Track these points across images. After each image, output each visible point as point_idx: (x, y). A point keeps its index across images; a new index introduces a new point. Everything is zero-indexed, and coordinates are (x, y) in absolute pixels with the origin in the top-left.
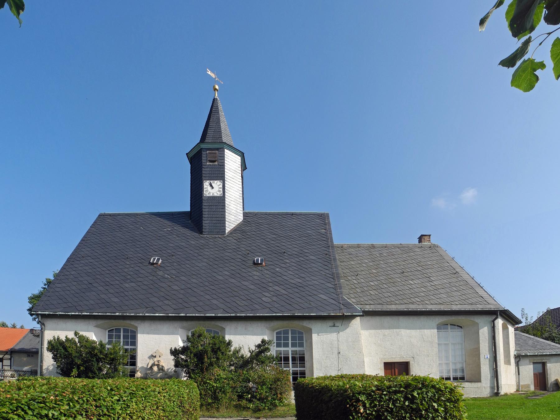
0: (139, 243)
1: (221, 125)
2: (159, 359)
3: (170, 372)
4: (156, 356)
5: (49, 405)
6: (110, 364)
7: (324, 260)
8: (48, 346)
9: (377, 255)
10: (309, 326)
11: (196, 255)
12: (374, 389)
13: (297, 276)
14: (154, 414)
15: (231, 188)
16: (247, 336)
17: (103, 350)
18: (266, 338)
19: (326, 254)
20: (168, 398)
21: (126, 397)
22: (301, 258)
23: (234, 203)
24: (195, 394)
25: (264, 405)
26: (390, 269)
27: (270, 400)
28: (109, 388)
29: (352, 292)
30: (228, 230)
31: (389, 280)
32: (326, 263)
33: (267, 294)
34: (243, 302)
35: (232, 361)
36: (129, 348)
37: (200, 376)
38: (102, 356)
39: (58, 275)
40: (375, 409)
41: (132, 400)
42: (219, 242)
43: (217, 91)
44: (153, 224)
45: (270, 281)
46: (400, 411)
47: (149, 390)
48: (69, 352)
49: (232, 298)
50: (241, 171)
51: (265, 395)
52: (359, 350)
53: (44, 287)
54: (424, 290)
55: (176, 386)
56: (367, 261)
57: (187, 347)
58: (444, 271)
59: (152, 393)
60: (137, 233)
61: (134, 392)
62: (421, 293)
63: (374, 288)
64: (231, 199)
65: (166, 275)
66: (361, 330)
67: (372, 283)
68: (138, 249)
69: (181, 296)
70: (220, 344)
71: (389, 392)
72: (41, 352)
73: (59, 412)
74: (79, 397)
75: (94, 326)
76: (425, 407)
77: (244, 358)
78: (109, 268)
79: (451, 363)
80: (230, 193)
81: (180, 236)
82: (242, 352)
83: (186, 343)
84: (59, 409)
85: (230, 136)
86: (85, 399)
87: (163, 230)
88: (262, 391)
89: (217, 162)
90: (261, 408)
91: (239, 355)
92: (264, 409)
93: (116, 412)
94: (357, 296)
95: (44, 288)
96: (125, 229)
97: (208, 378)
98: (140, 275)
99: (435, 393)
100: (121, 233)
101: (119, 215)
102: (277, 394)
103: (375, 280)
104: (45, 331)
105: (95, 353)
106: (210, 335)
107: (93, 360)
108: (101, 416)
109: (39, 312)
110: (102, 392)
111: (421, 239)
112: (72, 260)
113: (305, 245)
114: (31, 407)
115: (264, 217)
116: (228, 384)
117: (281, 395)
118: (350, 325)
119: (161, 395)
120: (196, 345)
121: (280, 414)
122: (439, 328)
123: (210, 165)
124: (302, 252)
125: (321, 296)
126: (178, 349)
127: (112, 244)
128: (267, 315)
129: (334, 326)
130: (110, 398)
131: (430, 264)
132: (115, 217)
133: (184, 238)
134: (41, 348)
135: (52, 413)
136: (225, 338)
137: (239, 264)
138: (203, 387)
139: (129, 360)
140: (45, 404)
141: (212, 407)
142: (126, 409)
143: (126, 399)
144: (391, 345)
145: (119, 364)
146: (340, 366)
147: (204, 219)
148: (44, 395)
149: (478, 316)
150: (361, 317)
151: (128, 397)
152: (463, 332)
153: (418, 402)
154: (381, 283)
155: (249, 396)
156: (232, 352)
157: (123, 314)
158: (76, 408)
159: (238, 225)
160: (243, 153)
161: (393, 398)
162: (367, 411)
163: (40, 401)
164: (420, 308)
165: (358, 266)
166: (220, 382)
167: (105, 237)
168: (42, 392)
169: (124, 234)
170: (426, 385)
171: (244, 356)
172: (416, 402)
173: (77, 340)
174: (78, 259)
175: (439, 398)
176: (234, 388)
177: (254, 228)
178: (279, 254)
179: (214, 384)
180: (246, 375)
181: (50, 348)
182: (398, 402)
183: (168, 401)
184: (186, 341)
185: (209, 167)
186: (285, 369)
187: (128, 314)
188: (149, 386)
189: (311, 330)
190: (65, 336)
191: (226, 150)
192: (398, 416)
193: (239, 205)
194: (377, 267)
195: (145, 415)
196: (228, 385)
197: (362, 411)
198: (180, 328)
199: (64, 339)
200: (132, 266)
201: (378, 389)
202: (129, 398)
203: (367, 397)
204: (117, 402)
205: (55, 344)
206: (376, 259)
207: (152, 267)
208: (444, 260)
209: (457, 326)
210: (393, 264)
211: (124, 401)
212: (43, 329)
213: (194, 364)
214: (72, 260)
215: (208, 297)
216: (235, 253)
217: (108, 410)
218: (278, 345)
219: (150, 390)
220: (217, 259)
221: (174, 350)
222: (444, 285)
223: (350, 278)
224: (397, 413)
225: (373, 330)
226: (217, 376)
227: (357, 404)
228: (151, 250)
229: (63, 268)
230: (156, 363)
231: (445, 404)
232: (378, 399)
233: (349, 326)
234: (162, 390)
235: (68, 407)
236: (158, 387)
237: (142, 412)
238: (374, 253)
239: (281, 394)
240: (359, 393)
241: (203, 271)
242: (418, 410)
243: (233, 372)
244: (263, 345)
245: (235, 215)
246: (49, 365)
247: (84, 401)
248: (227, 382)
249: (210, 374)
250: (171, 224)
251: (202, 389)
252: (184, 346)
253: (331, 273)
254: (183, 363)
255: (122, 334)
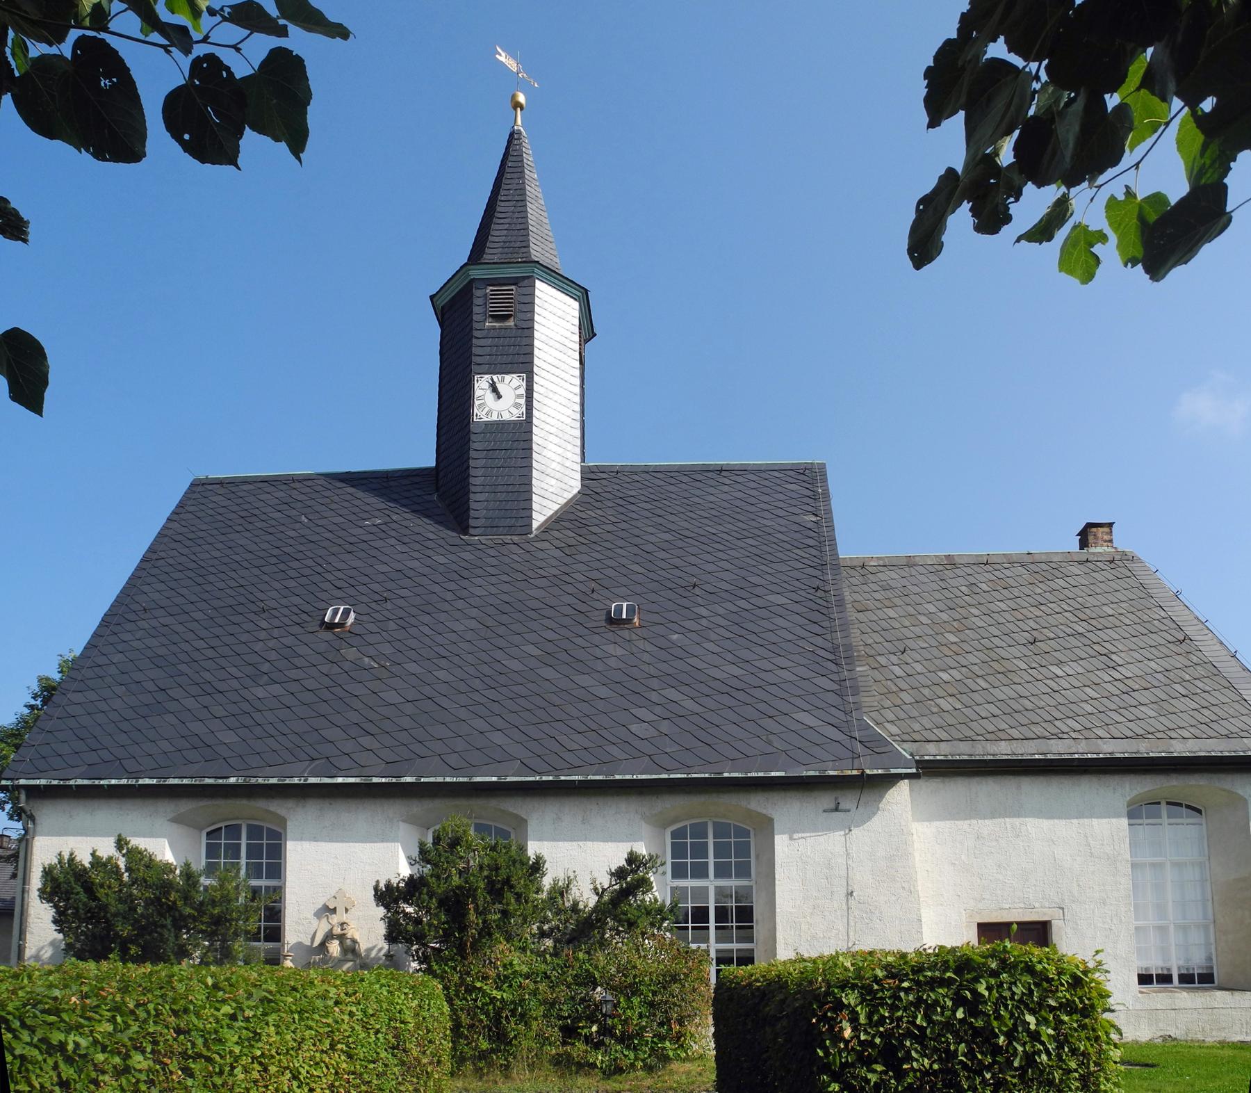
0: (295, 564)
1: (529, 209)
2: (344, 919)
3: (374, 958)
4: (335, 908)
5: (67, 1020)
6: (210, 936)
7: (810, 604)
8: (44, 885)
9: (963, 589)
10: (764, 812)
11: (449, 596)
12: (880, 973)
13: (730, 657)
14: (324, 1062)
15: (551, 395)
16: (589, 844)
17: (193, 893)
18: (642, 849)
19: (817, 589)
20: (362, 1019)
21: (251, 1010)
22: (742, 603)
23: (556, 440)
24: (436, 1015)
25: (632, 1055)
26: (997, 633)
27: (650, 1039)
28: (210, 981)
29: (887, 703)
30: (538, 519)
31: (992, 664)
32: (816, 617)
33: (641, 713)
34: (577, 737)
35: (545, 920)
36: (261, 887)
37: (455, 969)
38: (188, 911)
39: (75, 667)
40: (881, 1029)
41: (266, 1018)
42: (513, 556)
43: (522, 109)
44: (333, 506)
45: (653, 671)
46: (944, 1036)
47: (311, 993)
48: (99, 900)
49: (545, 727)
50: (580, 345)
51: (636, 1025)
52: (906, 885)
53: (33, 702)
54: (1093, 694)
55: (384, 988)
56: (932, 608)
57: (421, 878)
58: (1151, 635)
59: (319, 1003)
60: (292, 533)
61: (271, 997)
62: (1083, 705)
63: (952, 690)
64: (548, 428)
65: (366, 660)
66: (914, 820)
67: (945, 676)
68: (292, 583)
69: (406, 722)
70: (512, 868)
71: (918, 983)
72: (22, 906)
73: (91, 1038)
74: (137, 1001)
75: (169, 820)
76: (1006, 1025)
77: (580, 910)
78: (215, 642)
79: (1172, 926)
80: (545, 409)
81: (406, 540)
82: (574, 893)
83: (417, 866)
84: (92, 1032)
85: (550, 239)
86: (151, 1006)
87: (360, 523)
88: (629, 1013)
89: (512, 319)
90: (625, 1063)
91: (567, 904)
92: (632, 1065)
93: (227, 1049)
94: (902, 715)
95: (32, 707)
96: (259, 525)
97: (478, 973)
98: (296, 661)
99: (1032, 987)
100: (248, 535)
101: (245, 481)
102: (669, 1020)
103: (954, 664)
104: (36, 838)
105: (170, 901)
106: (482, 840)
107: (165, 922)
108: (188, 1059)
109: (22, 782)
110: (194, 991)
111: (1085, 536)
112: (116, 620)
113: (754, 563)
114: (28, 1022)
115: (639, 479)
116: (535, 993)
117: (680, 1025)
118: (880, 805)
119: (342, 1012)
120: (446, 870)
121: (678, 1082)
122: (1134, 812)
123: (494, 328)
124: (743, 584)
125: (801, 716)
126: (395, 885)
127: (224, 568)
128: (644, 777)
129: (836, 810)
130: (212, 1010)
131: (1111, 612)
132: (233, 489)
133: (417, 546)
134: (23, 891)
135: (74, 1041)
136: (526, 850)
137: (567, 621)
138: (464, 1002)
139: (262, 924)
140: (59, 1017)
141: (491, 1065)
142: (252, 1042)
143: (251, 1014)
144: (999, 866)
145: (236, 934)
146: (851, 934)
147: (472, 489)
148: (57, 993)
149: (963, 778)
150: (914, 781)
151: (257, 1008)
152: (1204, 825)
153: (989, 1011)
154: (970, 674)
155: (594, 1028)
156: (545, 894)
157: (248, 779)
158: (131, 1031)
159: (566, 504)
160: (586, 291)
161: (926, 1000)
162: (862, 1034)
163: (47, 1006)
164: (1081, 749)
165: (907, 624)
166: (510, 986)
167: (207, 547)
168: (51, 986)
169: (257, 539)
170: (1011, 962)
171: (581, 906)
172: (982, 1012)
173: (122, 863)
174: (132, 617)
175: (1042, 999)
176: (552, 1005)
177: (610, 511)
178: (681, 591)
179: (494, 992)
180: (584, 963)
181: (48, 890)
182: (939, 1010)
183: (360, 1029)
184: (417, 859)
185: (490, 335)
186: (694, 946)
187: (260, 781)
188: (312, 983)
189: (770, 821)
190: (91, 852)
191: (538, 284)
192: (939, 1050)
193: (569, 447)
194: (962, 627)
195: (301, 1066)
196: (535, 995)
197: (847, 1033)
198: (403, 821)
199: (85, 859)
200: (276, 633)
201: (893, 976)
202: (259, 1013)
203: (862, 994)
204: (228, 1022)
205: (62, 876)
206: (958, 601)
207: (327, 635)
208: (1152, 601)
209: (1188, 807)
210: (1007, 615)
211: (247, 1020)
212: (31, 832)
213: (439, 932)
214: (116, 620)
215: (479, 724)
216: (555, 591)
217: (206, 1044)
218: (678, 872)
219: (314, 992)
220: (507, 608)
221: (384, 889)
222: (1149, 678)
223: (882, 660)
224: (935, 1040)
225: (947, 822)
226: (505, 966)
227: (838, 1015)
228: (327, 586)
229: (90, 646)
230: (337, 931)
231: (1057, 1018)
232: (889, 1002)
233: (878, 809)
234: (346, 994)
235: (110, 1028)
236: (335, 987)
237: (292, 1056)
238: (953, 582)
239: (680, 1021)
240: (843, 988)
241: (466, 646)
242: (986, 1036)
243: (548, 956)
244: (632, 871)
245: (558, 475)
246: (42, 944)
247: (148, 1012)
248: (532, 986)
249: (485, 961)
250: (383, 506)
251: (462, 1009)
252: (411, 876)
253: (830, 645)
254: (410, 928)
255: (244, 842)
